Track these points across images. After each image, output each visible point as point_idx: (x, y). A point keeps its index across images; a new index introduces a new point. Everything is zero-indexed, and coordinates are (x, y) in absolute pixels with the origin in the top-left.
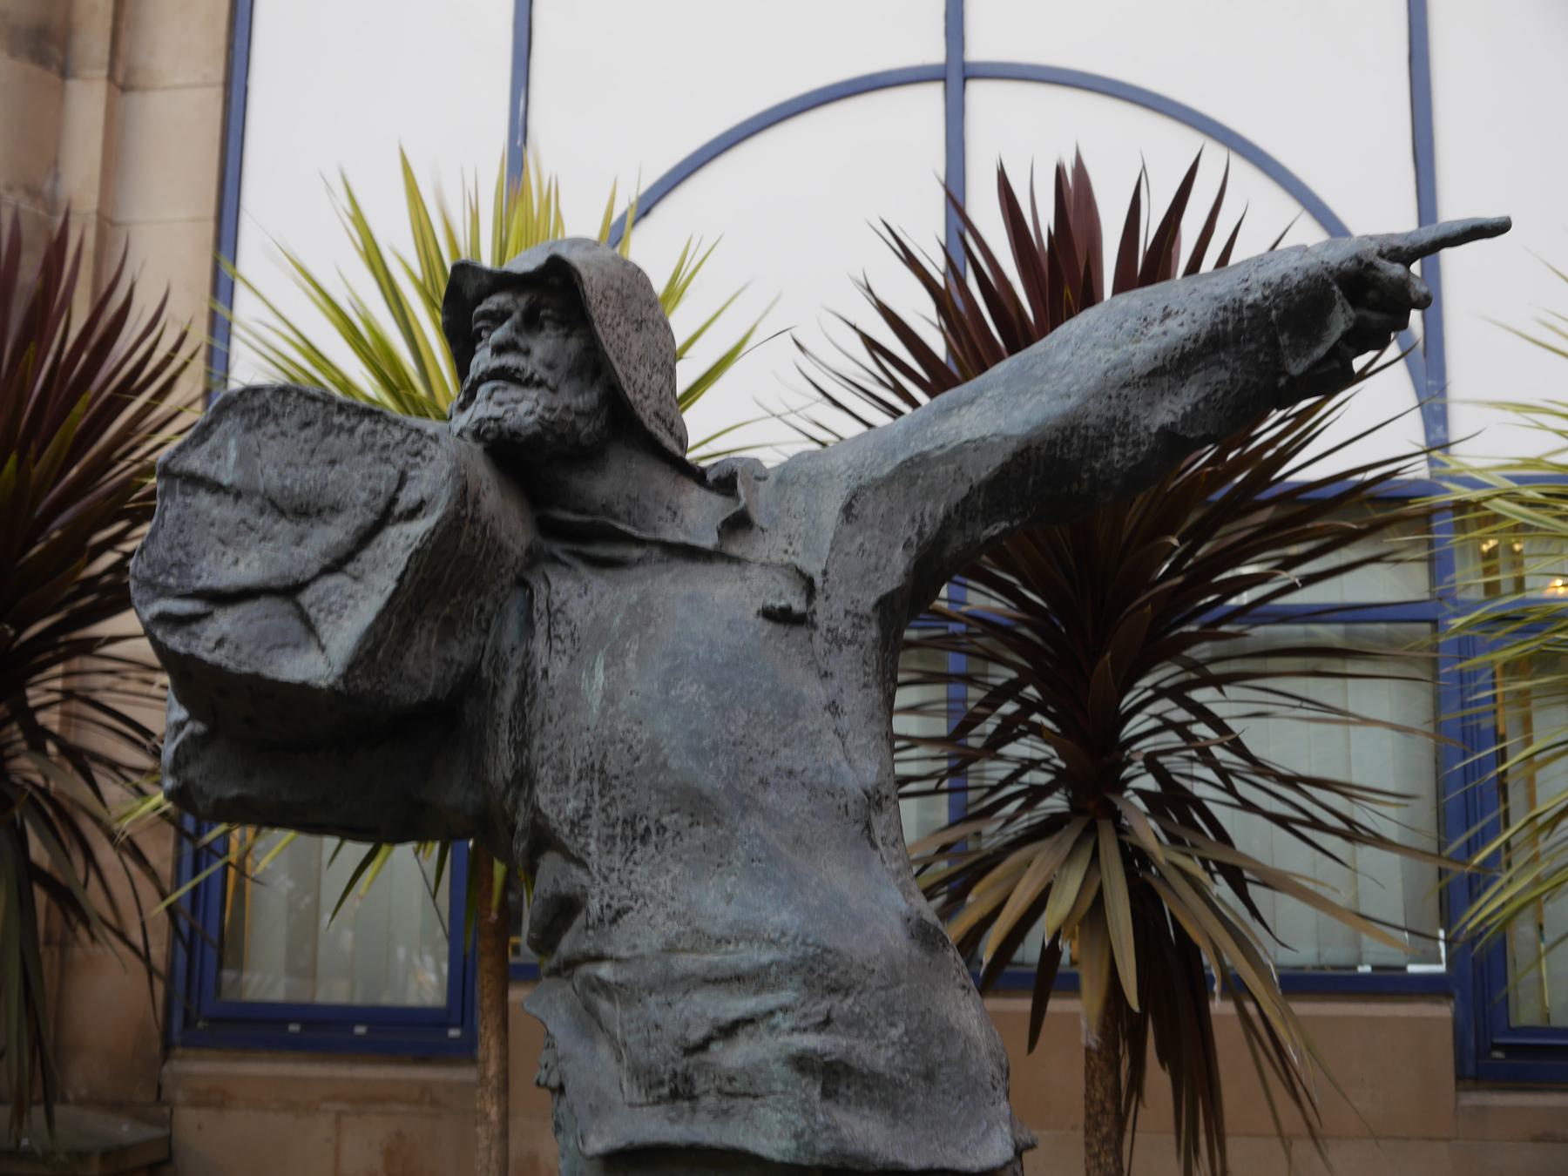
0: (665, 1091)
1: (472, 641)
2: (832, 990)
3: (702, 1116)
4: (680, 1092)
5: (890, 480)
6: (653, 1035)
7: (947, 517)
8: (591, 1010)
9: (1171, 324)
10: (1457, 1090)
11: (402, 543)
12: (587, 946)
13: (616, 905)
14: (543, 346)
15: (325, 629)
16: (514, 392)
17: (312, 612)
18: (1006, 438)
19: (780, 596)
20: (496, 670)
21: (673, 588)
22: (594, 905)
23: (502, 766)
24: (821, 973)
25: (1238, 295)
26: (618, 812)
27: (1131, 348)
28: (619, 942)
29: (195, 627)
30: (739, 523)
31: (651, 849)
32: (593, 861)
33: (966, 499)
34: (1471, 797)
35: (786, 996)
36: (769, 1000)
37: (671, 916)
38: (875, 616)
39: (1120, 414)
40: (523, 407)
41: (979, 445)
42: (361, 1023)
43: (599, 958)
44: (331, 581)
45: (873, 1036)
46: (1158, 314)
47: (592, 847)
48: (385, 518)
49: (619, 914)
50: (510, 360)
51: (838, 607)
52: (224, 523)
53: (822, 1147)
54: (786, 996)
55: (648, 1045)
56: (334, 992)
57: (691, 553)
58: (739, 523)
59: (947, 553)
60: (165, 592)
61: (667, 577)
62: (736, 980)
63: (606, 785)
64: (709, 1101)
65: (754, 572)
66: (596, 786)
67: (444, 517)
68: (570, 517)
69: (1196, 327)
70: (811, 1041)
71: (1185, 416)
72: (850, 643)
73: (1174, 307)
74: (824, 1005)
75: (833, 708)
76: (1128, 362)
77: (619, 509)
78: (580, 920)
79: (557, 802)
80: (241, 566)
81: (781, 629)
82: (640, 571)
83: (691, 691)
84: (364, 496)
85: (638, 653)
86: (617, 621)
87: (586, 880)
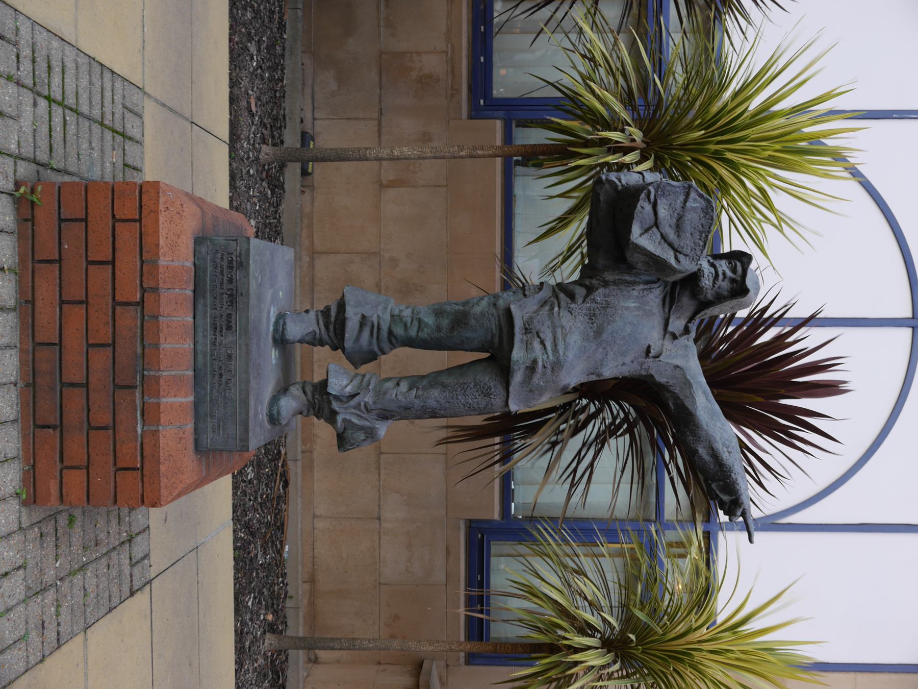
4: (527, 331)
5: (685, 377)
8: (545, 303)
9: (727, 454)
12: (562, 303)
16: (711, 280)
21: (656, 322)
22: (573, 306)
23: (609, 276)
24: (557, 366)
26: (597, 312)
28: (564, 313)
30: (674, 337)
32: (584, 305)
34: (584, 531)
35: (551, 357)
36: (550, 353)
40: (707, 282)
41: (694, 402)
42: (485, 59)
43: (559, 307)
44: (659, 236)
48: (676, 250)
50: (721, 277)
51: (651, 364)
54: (551, 357)
56: (499, 42)
57: (666, 325)
60: (656, 191)
62: (555, 345)
63: (604, 308)
64: (525, 338)
65: (661, 342)
68: (677, 290)
70: (540, 364)
75: (624, 364)
78: (569, 301)
79: (600, 294)
83: (628, 329)
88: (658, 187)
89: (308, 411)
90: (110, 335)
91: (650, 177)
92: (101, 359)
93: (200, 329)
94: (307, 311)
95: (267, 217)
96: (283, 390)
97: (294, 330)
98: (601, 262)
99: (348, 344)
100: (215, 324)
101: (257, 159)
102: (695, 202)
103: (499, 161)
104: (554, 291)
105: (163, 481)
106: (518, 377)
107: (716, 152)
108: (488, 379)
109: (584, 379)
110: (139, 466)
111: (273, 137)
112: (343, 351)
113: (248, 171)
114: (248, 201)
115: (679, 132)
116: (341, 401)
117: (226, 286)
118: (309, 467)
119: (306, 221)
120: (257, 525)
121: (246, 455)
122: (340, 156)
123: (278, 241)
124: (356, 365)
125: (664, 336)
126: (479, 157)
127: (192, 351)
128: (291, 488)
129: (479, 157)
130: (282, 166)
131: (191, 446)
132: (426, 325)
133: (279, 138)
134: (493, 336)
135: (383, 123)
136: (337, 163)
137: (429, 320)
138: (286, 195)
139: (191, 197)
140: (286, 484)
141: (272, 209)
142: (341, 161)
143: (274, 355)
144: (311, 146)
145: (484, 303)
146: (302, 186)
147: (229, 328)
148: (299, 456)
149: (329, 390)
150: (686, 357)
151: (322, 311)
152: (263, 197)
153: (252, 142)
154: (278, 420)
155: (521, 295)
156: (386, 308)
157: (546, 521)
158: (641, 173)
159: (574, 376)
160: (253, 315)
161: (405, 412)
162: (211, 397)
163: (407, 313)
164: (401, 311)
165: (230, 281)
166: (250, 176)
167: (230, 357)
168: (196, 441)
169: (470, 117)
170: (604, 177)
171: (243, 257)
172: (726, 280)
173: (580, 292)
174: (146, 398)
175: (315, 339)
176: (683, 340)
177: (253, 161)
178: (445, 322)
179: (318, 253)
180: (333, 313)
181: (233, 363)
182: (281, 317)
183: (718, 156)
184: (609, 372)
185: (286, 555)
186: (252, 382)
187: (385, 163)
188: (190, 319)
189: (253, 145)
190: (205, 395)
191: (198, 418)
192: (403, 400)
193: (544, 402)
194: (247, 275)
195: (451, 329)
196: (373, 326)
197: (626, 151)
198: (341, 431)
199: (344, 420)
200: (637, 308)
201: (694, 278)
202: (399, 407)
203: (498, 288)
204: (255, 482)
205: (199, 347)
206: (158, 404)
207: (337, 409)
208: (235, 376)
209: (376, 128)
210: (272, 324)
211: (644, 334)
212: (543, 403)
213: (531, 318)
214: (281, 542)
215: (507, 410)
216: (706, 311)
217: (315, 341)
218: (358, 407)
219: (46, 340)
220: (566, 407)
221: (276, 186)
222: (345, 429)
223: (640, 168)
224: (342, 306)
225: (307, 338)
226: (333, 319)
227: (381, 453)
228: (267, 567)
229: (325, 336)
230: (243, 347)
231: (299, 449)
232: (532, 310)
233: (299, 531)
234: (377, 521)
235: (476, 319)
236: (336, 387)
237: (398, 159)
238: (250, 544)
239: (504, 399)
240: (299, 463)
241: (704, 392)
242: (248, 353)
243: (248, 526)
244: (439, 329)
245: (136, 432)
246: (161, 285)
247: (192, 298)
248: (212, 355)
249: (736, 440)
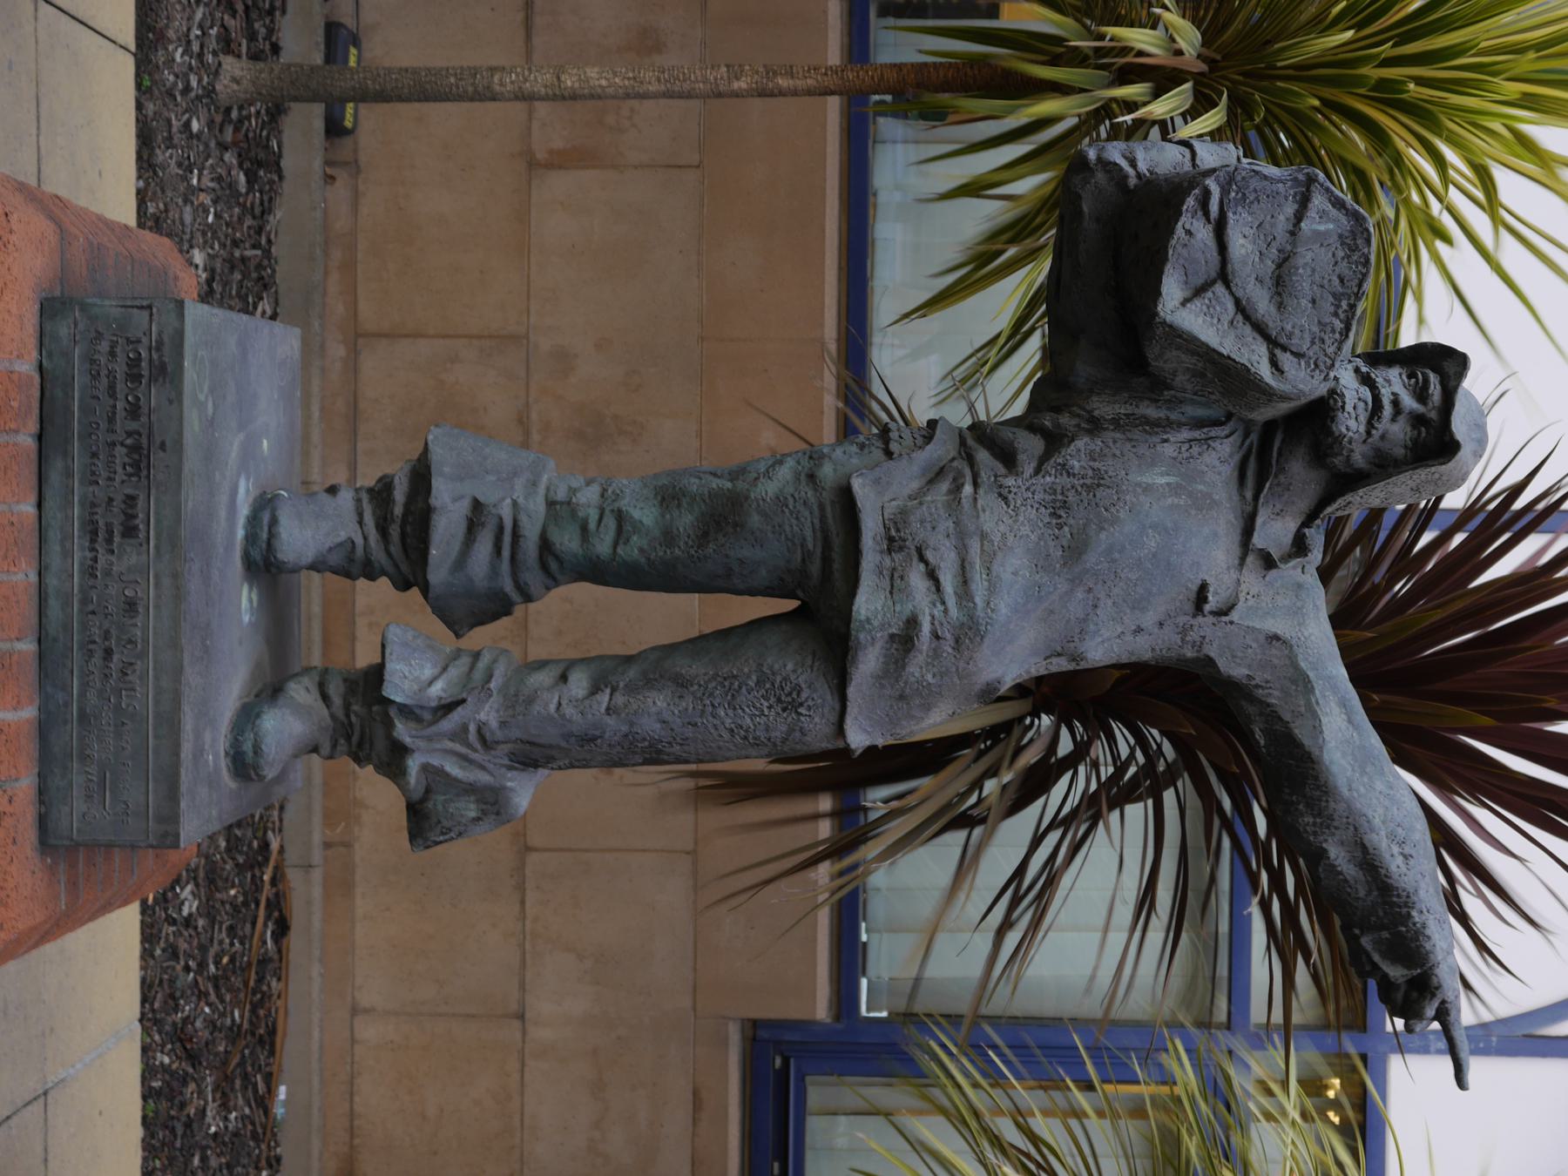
0: (893, 533)
1: (1189, 387)
2: (957, 641)
3: (878, 558)
4: (893, 544)
5: (1296, 667)
6: (928, 526)
7: (1268, 705)
9: (1400, 860)
10: (743, 1020)
11: (1255, 358)
12: (984, 476)
13: (1011, 497)
15: (1197, 304)
16: (1363, 418)
17: (1209, 294)
18: (1321, 748)
19: (1216, 593)
20: (1170, 401)
21: (1225, 524)
22: (1010, 481)
23: (1103, 407)
24: (969, 633)
25: (1418, 906)
26: (1072, 497)
27: (1383, 833)
28: (987, 499)
29: (1200, 213)
31: (1047, 520)
32: (1039, 479)
33: (1280, 718)
34: (1046, 1048)
35: (954, 611)
36: (951, 602)
37: (1004, 536)
38: (1201, 655)
39: (1336, 824)
40: (1352, 424)
41: (1317, 729)
43: (976, 485)
44: (1231, 306)
45: (928, 664)
46: (1407, 850)
47: (1048, 479)
48: (1273, 343)
49: (1005, 499)
51: (1208, 632)
52: (1273, 225)
53: (862, 636)
54: (954, 611)
55: (922, 522)
57: (1248, 531)
58: (1268, 562)
59: (1243, 703)
60: (1225, 191)
61: (1231, 517)
62: (964, 581)
63: (1089, 488)
64: (887, 562)
65: (1234, 575)
66: (1088, 481)
67: (1271, 388)
69: (1396, 877)
70: (926, 628)
71: (1334, 866)
72: (1183, 640)
73: (1412, 862)
74: (948, 636)
76: (1372, 830)
77: (1282, 478)
78: (1001, 469)
79: (1078, 453)
80: (1242, 241)
81: (1193, 596)
82: (1236, 498)
83: (1152, 542)
84: (1289, 327)
85: (1178, 506)
86: (1201, 487)
87: (1027, 474)
88: (1230, 180)
89: (334, 746)
91: (1210, 155)
93: (54, 535)
94: (332, 490)
95: (236, 243)
96: (270, 689)
97: (300, 537)
98: (1084, 370)
99: (438, 572)
100: (94, 523)
101: (210, 92)
102: (1322, 221)
103: (834, 104)
104: (963, 442)
106: (868, 663)
107: (1383, 84)
108: (793, 665)
109: (1038, 668)
111: (252, 37)
112: (425, 590)
113: (187, 125)
114: (186, 201)
115: (1294, 35)
116: (419, 720)
117: (122, 424)
118: (341, 885)
119: (337, 255)
120: (206, 1034)
121: (173, 856)
122: (424, 89)
123: (265, 305)
124: (457, 626)
125: (1243, 560)
126: (782, 93)
127: (34, 591)
128: (295, 940)
129: (782, 93)
130: (276, 112)
131: (30, 835)
132: (637, 527)
133: (268, 37)
134: (807, 556)
136: (417, 105)
137: (645, 514)
138: (287, 187)
139: (34, 196)
140: (282, 928)
141: (248, 222)
142: (427, 99)
143: (246, 601)
144: (352, 62)
145: (785, 472)
146: (328, 163)
147: (130, 531)
148: (317, 856)
149: (389, 692)
150: (1296, 612)
151: (370, 491)
152: (225, 191)
153: (196, 48)
154: (256, 768)
155: (878, 454)
156: (535, 484)
157: (938, 1024)
158: (1183, 139)
159: (1012, 660)
160: (191, 499)
161: (581, 749)
163: (589, 497)
164: (573, 491)
165: (134, 411)
166: (191, 136)
167: (131, 606)
168: (43, 822)
170: (1092, 155)
171: (166, 350)
172: (1402, 419)
173: (1029, 446)
175: (351, 560)
176: (1290, 571)
177: (198, 98)
178: (685, 521)
180: (399, 495)
181: (139, 621)
182: (265, 504)
183: (1389, 96)
184: (1100, 651)
185: (279, 1111)
186: (188, 670)
187: (542, 109)
188: (28, 508)
189: (201, 56)
190: (67, 704)
191: (48, 761)
192: (577, 717)
193: (935, 723)
194: (177, 399)
195: (699, 540)
196: (500, 529)
197: (1163, 80)
198: (417, 795)
199: (426, 768)
200: (1175, 490)
201: (1318, 414)
202: (567, 736)
203: (829, 433)
204: (201, 923)
205: (52, 582)
207: (407, 740)
208: (143, 655)
209: (520, 16)
210: (241, 521)
211: (1191, 555)
212: (935, 725)
213: (904, 512)
214: (268, 1078)
215: (841, 744)
216: (1348, 497)
217: (351, 565)
218: (460, 734)
220: (996, 733)
221: (260, 164)
222: (428, 791)
223: (1188, 131)
224: (421, 476)
225: (334, 559)
226: (398, 510)
227: (529, 849)
228: (229, 1142)
229: (378, 555)
231: (317, 838)
232: (907, 492)
233: (315, 1046)
234: (516, 1024)
235: (764, 514)
236: (406, 685)
237: (574, 97)
238: (185, 1083)
239: (833, 718)
240: (317, 875)
241: (1343, 704)
242: (179, 595)
243: (180, 1037)
244: (669, 537)
247: (34, 456)
248: (85, 601)
249: (1422, 825)
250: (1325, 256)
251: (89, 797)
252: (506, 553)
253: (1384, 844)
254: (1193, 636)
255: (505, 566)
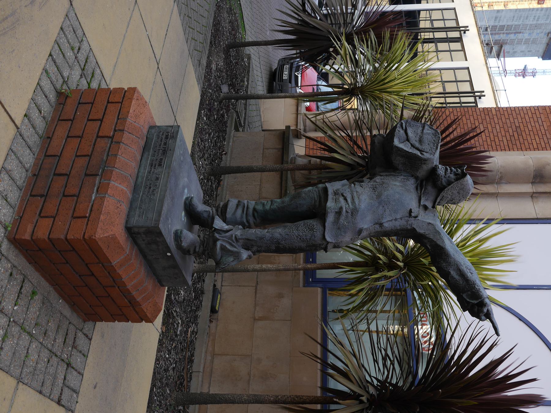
2: (352, 213)
5: (436, 230)
14: (452, 176)
26: (377, 186)
35: (351, 206)
36: (350, 204)
41: (443, 241)
44: (410, 145)
51: (413, 222)
54: (351, 206)
58: (426, 208)
60: (406, 124)
70: (344, 210)
79: (378, 179)
83: (397, 196)
90: (90, 152)
92: (81, 162)
93: (143, 166)
99: (229, 215)
105: (100, 225)
106: (330, 218)
110: (87, 215)
135: (258, 288)
147: (160, 165)
162: (141, 198)
165: (165, 144)
167: (157, 179)
169: (304, 286)
174: (102, 180)
179: (216, 355)
191: (131, 208)
196: (244, 206)
205: (140, 174)
206: (109, 184)
219: (53, 154)
230: (166, 174)
245: (91, 197)
246: (126, 129)
248: (147, 178)
250: (430, 137)
251: (139, 216)
252: (245, 212)
253: (465, 269)
254: (410, 223)
255: (244, 215)
